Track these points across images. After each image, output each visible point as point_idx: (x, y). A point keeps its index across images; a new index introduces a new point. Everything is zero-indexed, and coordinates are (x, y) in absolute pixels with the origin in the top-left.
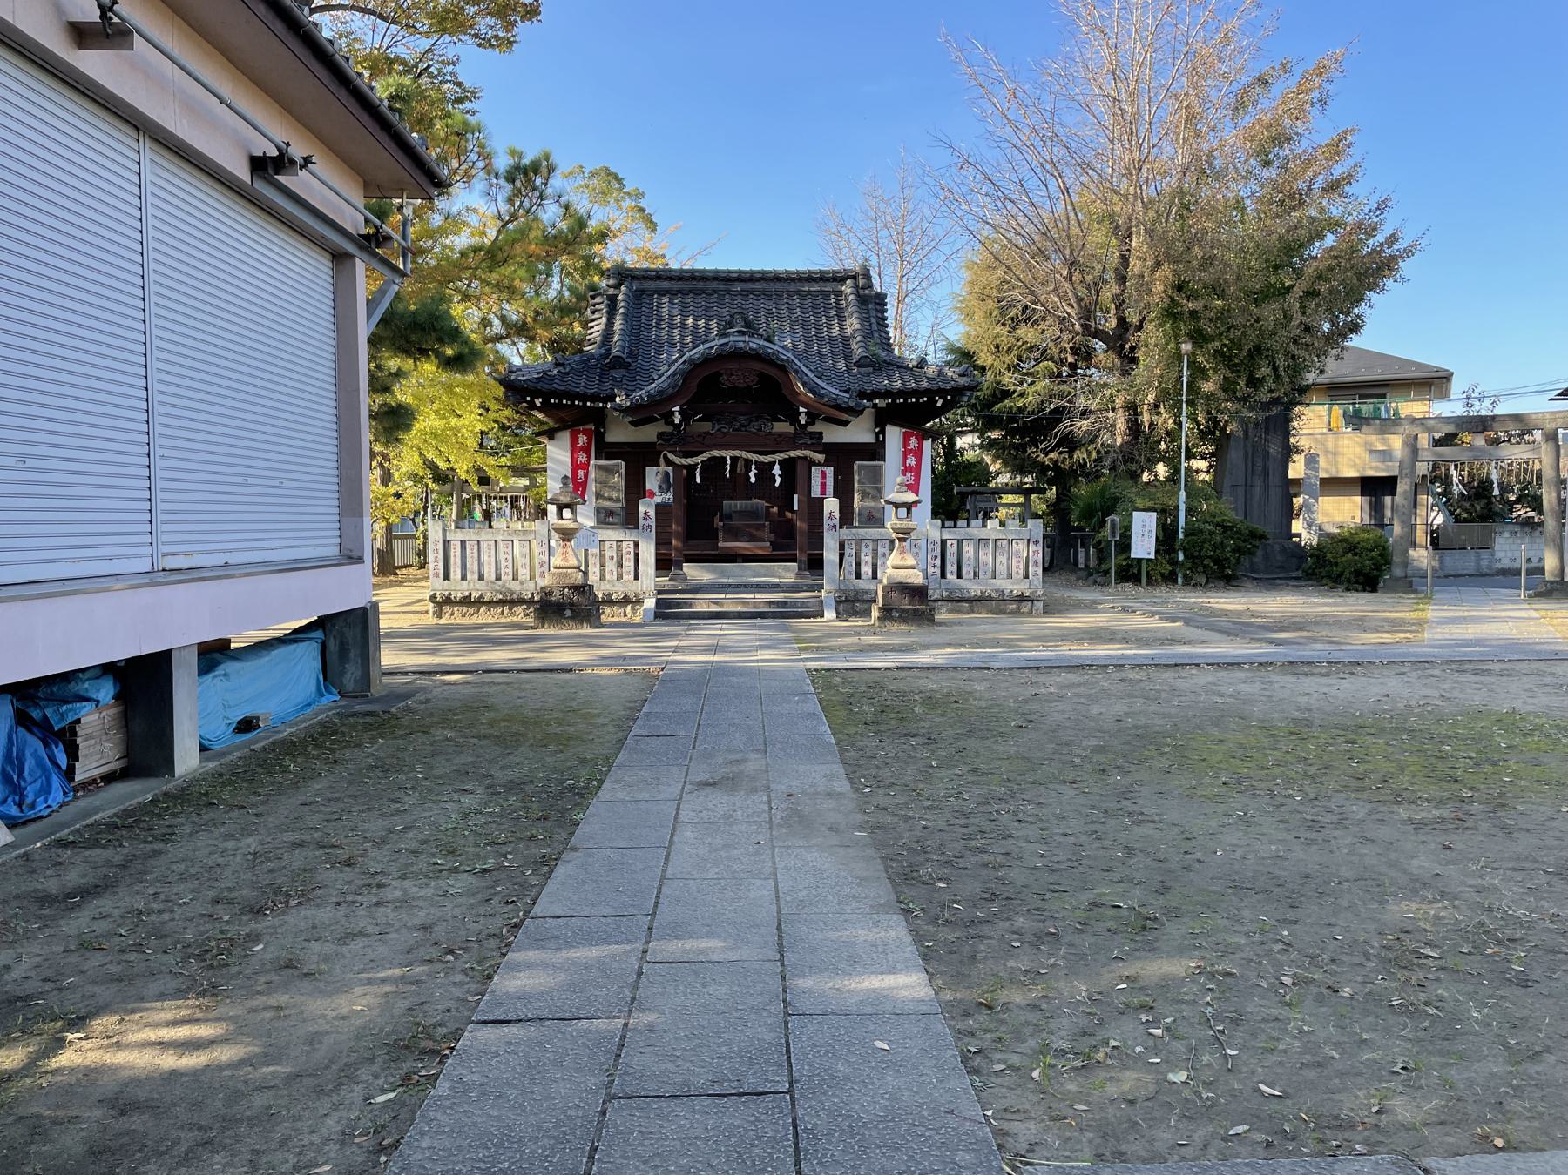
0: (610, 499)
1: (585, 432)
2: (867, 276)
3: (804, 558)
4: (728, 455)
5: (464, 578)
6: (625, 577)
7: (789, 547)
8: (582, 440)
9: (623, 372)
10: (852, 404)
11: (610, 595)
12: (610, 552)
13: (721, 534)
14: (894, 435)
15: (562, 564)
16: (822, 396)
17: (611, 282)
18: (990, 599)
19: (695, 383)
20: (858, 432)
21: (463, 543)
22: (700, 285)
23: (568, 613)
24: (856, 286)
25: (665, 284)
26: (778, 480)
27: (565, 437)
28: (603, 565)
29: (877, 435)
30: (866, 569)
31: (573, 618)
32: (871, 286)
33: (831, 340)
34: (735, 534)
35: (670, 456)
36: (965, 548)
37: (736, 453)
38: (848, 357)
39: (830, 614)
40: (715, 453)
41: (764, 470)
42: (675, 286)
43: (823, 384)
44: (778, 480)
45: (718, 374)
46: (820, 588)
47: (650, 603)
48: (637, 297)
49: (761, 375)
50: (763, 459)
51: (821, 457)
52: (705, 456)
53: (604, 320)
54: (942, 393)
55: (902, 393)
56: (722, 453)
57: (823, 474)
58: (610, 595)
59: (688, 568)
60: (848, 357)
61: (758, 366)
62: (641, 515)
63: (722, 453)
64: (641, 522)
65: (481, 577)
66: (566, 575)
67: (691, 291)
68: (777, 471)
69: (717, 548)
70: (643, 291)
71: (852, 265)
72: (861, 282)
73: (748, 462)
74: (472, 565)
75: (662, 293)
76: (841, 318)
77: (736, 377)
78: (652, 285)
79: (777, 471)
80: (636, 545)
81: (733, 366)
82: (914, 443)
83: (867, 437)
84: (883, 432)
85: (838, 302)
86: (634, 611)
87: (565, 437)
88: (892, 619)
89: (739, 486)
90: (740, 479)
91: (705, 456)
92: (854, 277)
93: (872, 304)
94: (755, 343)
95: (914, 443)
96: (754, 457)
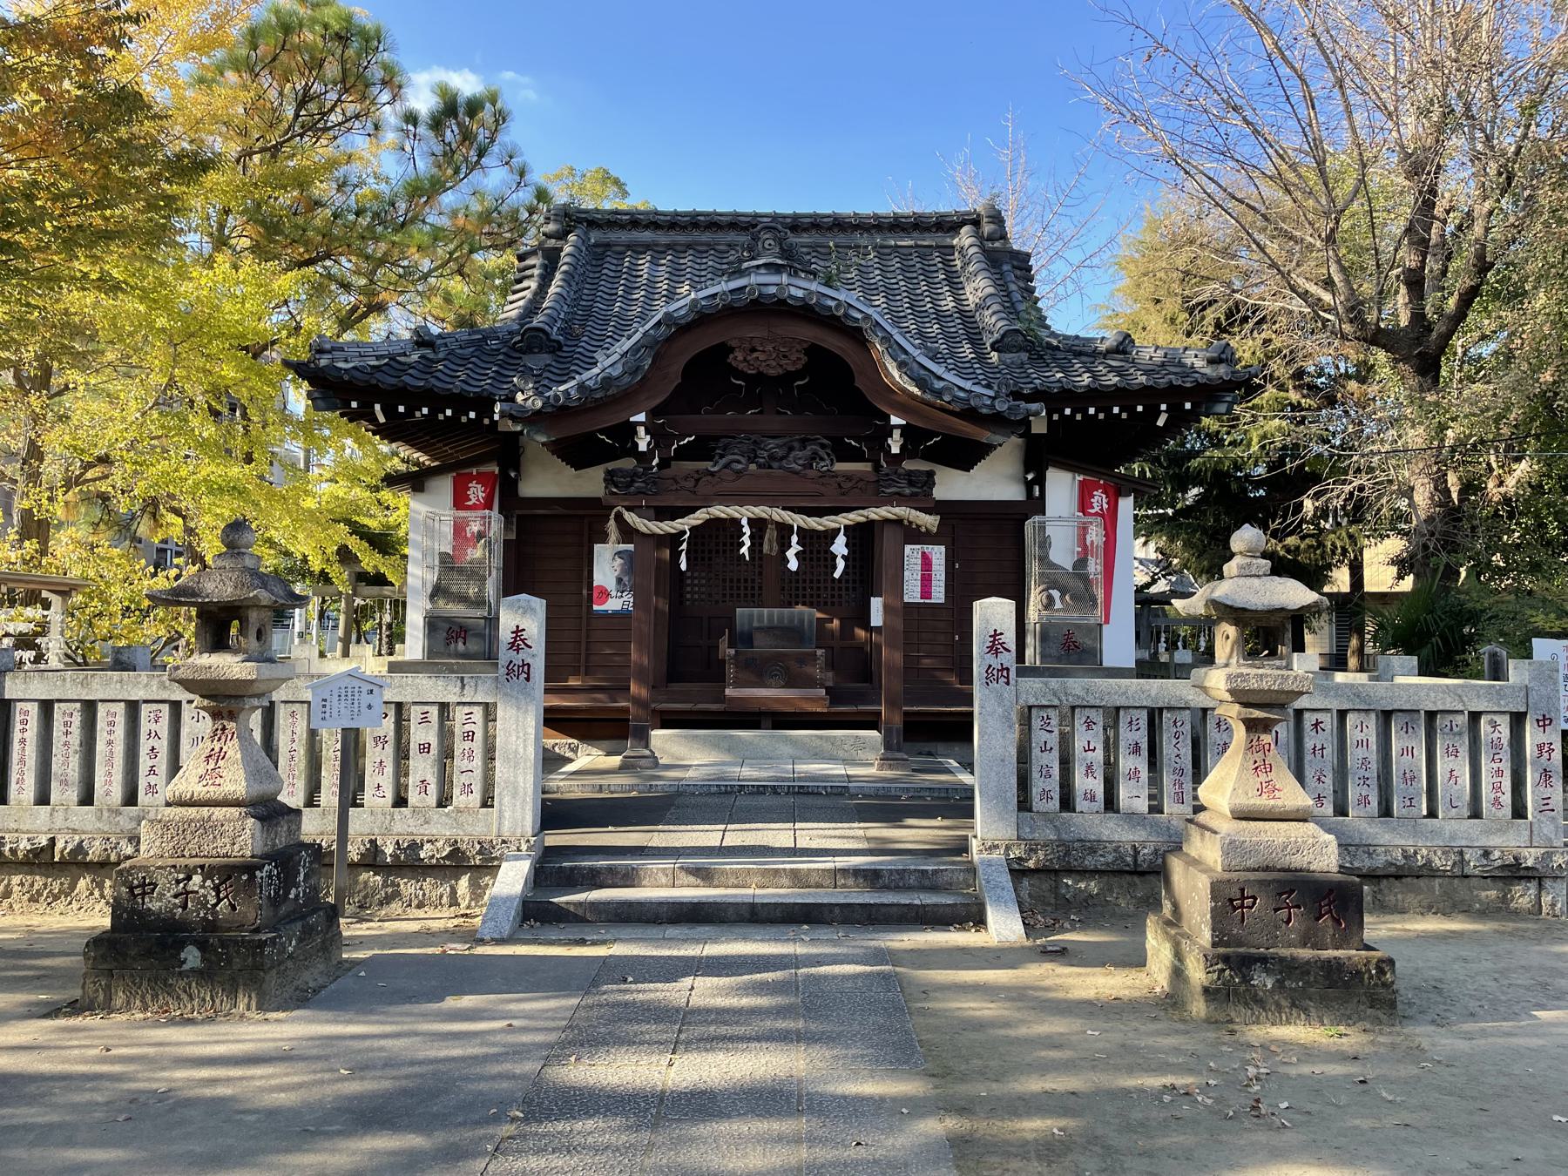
0: (463, 599)
1: (480, 478)
2: (997, 218)
3: (898, 721)
4: (744, 513)
5: (43, 799)
6: (459, 799)
7: (861, 698)
8: (476, 492)
9: (546, 359)
10: (1001, 406)
11: (415, 847)
12: (423, 734)
13: (731, 670)
14: (1061, 488)
15: (200, 791)
16: (939, 393)
17: (551, 227)
18: (1429, 872)
19: (676, 368)
20: (991, 481)
21: (47, 707)
22: (706, 237)
23: (192, 957)
24: (978, 235)
25: (647, 236)
26: (841, 564)
27: (444, 487)
28: (401, 771)
29: (1029, 486)
30: (1088, 784)
31: (205, 975)
32: (1004, 237)
33: (940, 316)
34: (759, 671)
35: (630, 517)
36: (1353, 734)
37: (760, 511)
38: (976, 342)
39: (1004, 925)
40: (719, 511)
41: (816, 544)
42: (663, 238)
43: (939, 370)
44: (841, 564)
45: (724, 350)
46: (958, 805)
47: (512, 878)
48: (596, 256)
49: (814, 351)
50: (813, 523)
51: (930, 521)
52: (699, 517)
53: (533, 284)
54: (1174, 394)
55: (1096, 395)
56: (732, 511)
57: (926, 562)
58: (415, 847)
59: (663, 740)
60: (975, 339)
61: (810, 333)
62: (505, 634)
63: (732, 511)
64: (505, 655)
65: (87, 799)
66: (205, 826)
67: (689, 246)
68: (839, 547)
69: (722, 698)
70: (608, 246)
71: (972, 202)
72: (987, 228)
73: (784, 530)
74: (66, 764)
75: (639, 249)
76: (955, 286)
77: (765, 353)
78: (623, 236)
79: (839, 547)
80: (489, 712)
81: (753, 331)
82: (1099, 500)
83: (1011, 492)
84: (1041, 481)
85: (947, 263)
86: (477, 891)
87: (444, 487)
88: (1255, 1000)
89: (763, 579)
90: (767, 562)
91: (699, 517)
92: (976, 223)
93: (1010, 267)
94: (799, 288)
95: (1099, 500)
96: (797, 520)
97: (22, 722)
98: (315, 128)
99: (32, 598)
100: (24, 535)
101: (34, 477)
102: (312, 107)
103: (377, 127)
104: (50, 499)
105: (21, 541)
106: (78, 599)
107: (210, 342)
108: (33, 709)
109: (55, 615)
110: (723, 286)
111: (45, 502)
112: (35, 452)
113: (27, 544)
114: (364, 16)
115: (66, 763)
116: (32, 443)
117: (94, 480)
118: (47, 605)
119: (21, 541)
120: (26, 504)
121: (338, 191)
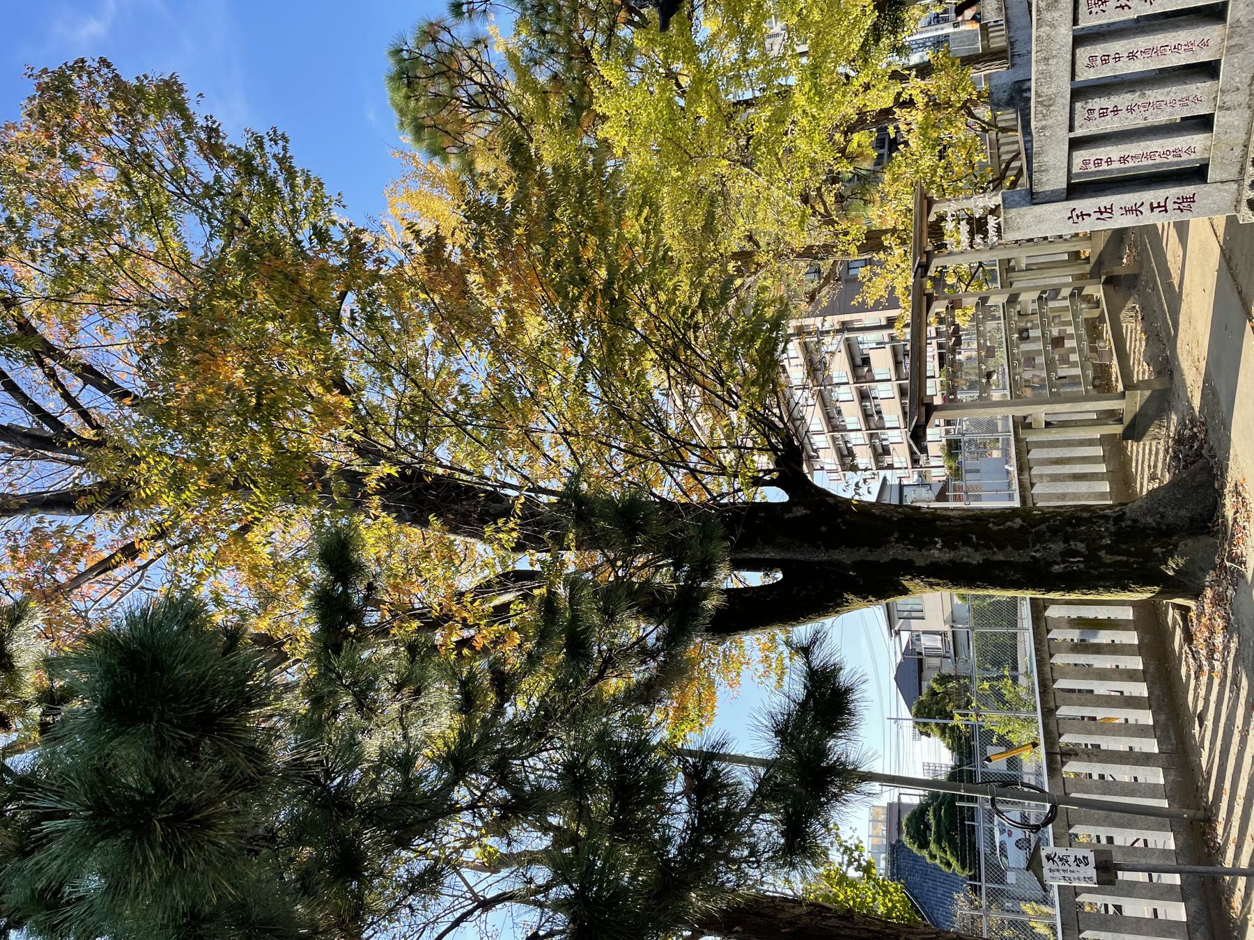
97: (1099, 165)
98: (491, 90)
99: (936, 230)
100: (880, 247)
101: (828, 249)
102: (481, 100)
103: (477, 42)
104: (846, 234)
105: (885, 249)
106: (933, 193)
107: (680, 129)
108: (1080, 156)
109: (948, 208)
110: (1161, 862)
111: (849, 238)
112: (808, 252)
113: (886, 243)
114: (390, 65)
115: (1157, 105)
116: (799, 256)
117: (824, 204)
118: (942, 218)
119: (885, 249)
120: (853, 249)
121: (541, 64)
